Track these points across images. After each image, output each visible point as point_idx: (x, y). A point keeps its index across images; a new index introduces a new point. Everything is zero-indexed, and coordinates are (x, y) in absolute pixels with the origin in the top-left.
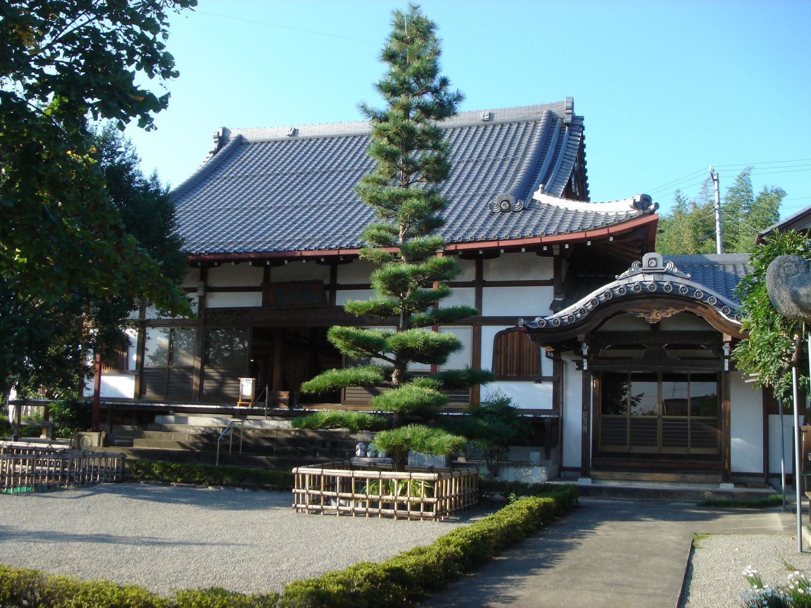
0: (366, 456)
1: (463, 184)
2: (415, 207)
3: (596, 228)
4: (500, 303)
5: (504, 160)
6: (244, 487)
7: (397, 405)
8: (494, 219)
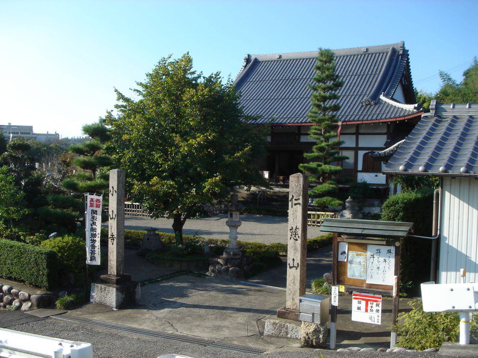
0: (312, 203)
1: (353, 88)
2: (327, 124)
3: (400, 117)
4: (366, 142)
5: (371, 75)
6: (270, 215)
7: (321, 191)
8: (363, 109)
